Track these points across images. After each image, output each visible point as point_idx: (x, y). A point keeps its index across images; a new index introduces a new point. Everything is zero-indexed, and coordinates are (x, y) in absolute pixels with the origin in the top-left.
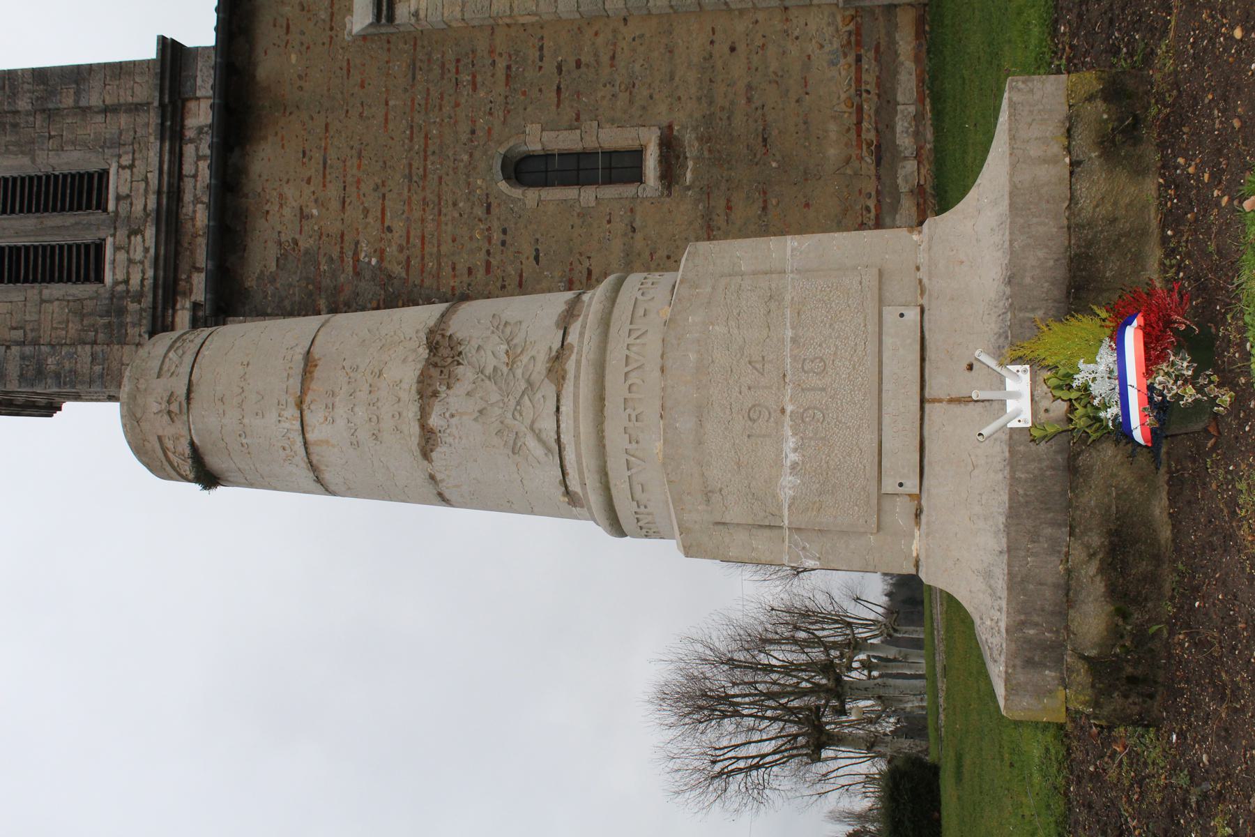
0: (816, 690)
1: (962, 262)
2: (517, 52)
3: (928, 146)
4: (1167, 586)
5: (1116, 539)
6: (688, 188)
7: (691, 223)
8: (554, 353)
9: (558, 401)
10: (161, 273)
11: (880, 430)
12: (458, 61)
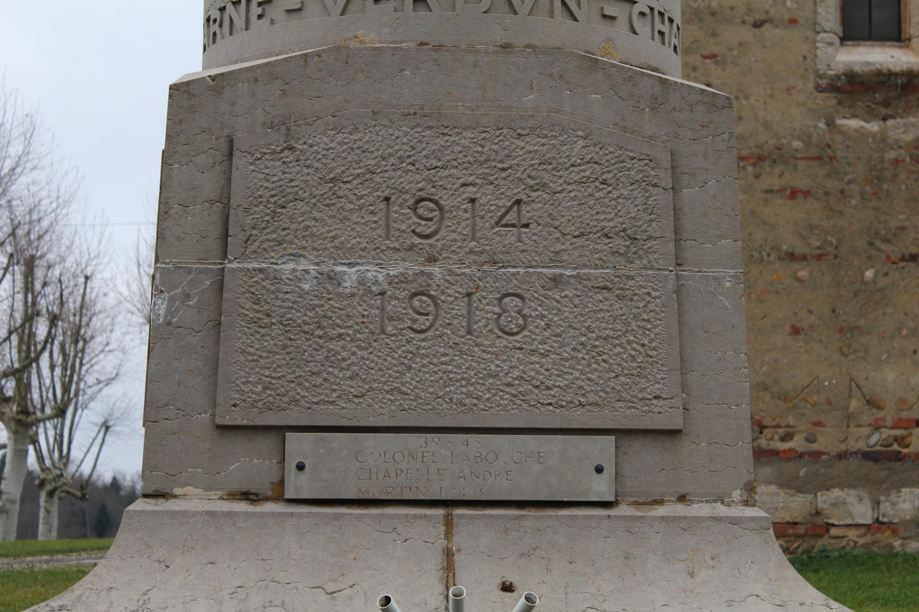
1: (692, 575)
3: (897, 543)
6: (830, 124)
7: (767, 126)
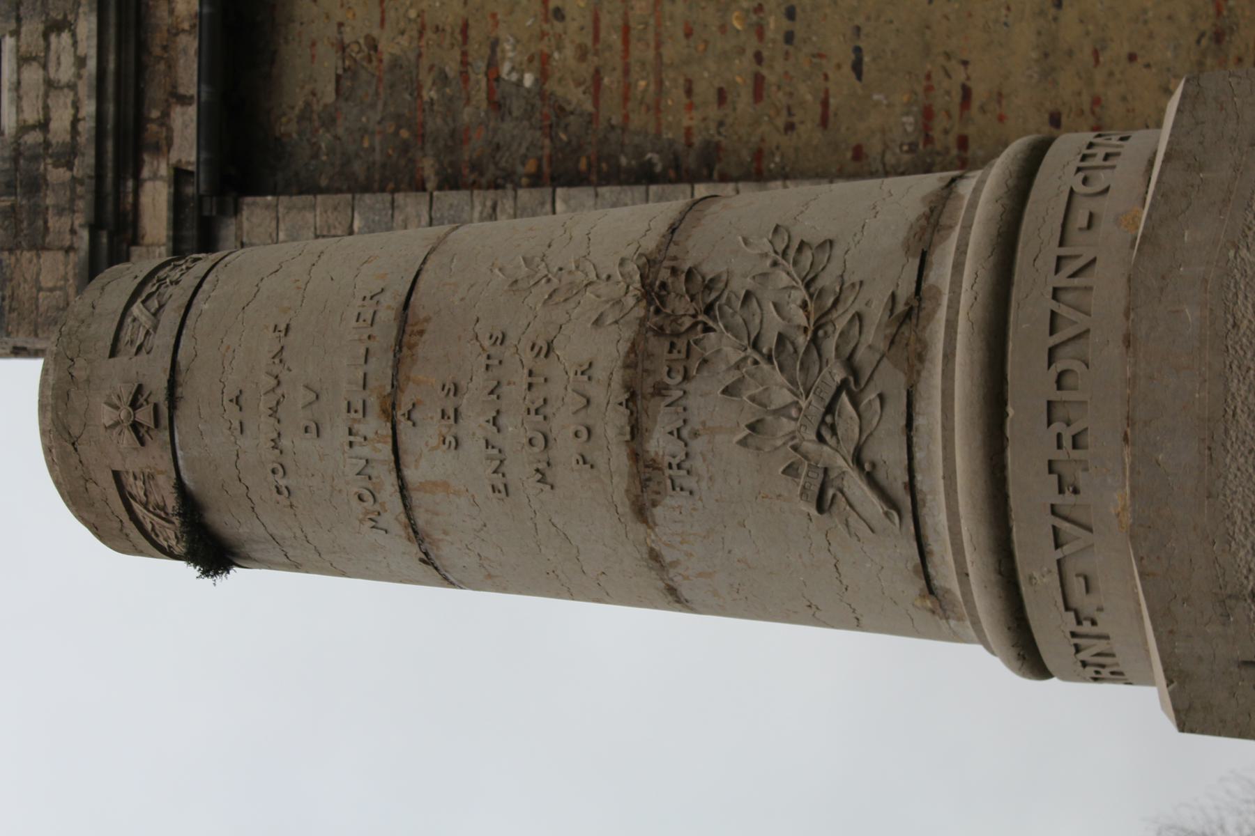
8: (901, 308)
10: (111, 108)
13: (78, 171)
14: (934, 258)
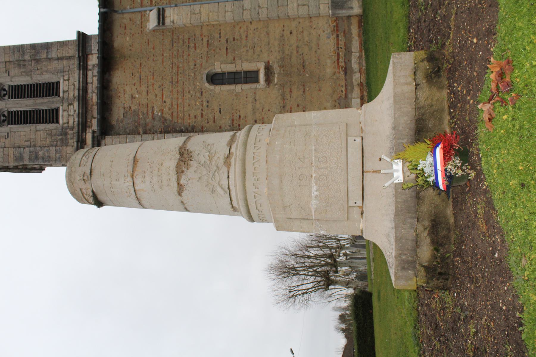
0: (327, 264)
2: (211, 35)
3: (364, 68)
4: (452, 240)
5: (434, 223)
6: (276, 85)
7: (277, 98)
8: (226, 156)
9: (228, 173)
10: (80, 120)
11: (348, 183)
12: (189, 39)
13: (74, 131)
14: (232, 147)
